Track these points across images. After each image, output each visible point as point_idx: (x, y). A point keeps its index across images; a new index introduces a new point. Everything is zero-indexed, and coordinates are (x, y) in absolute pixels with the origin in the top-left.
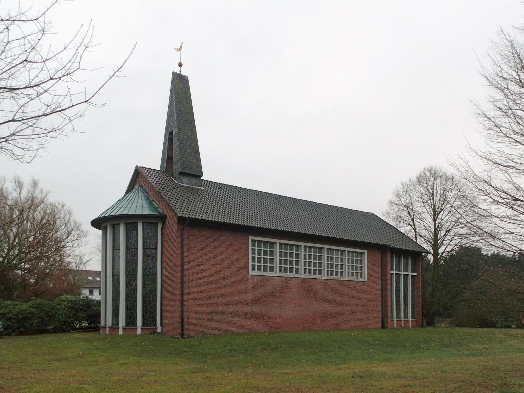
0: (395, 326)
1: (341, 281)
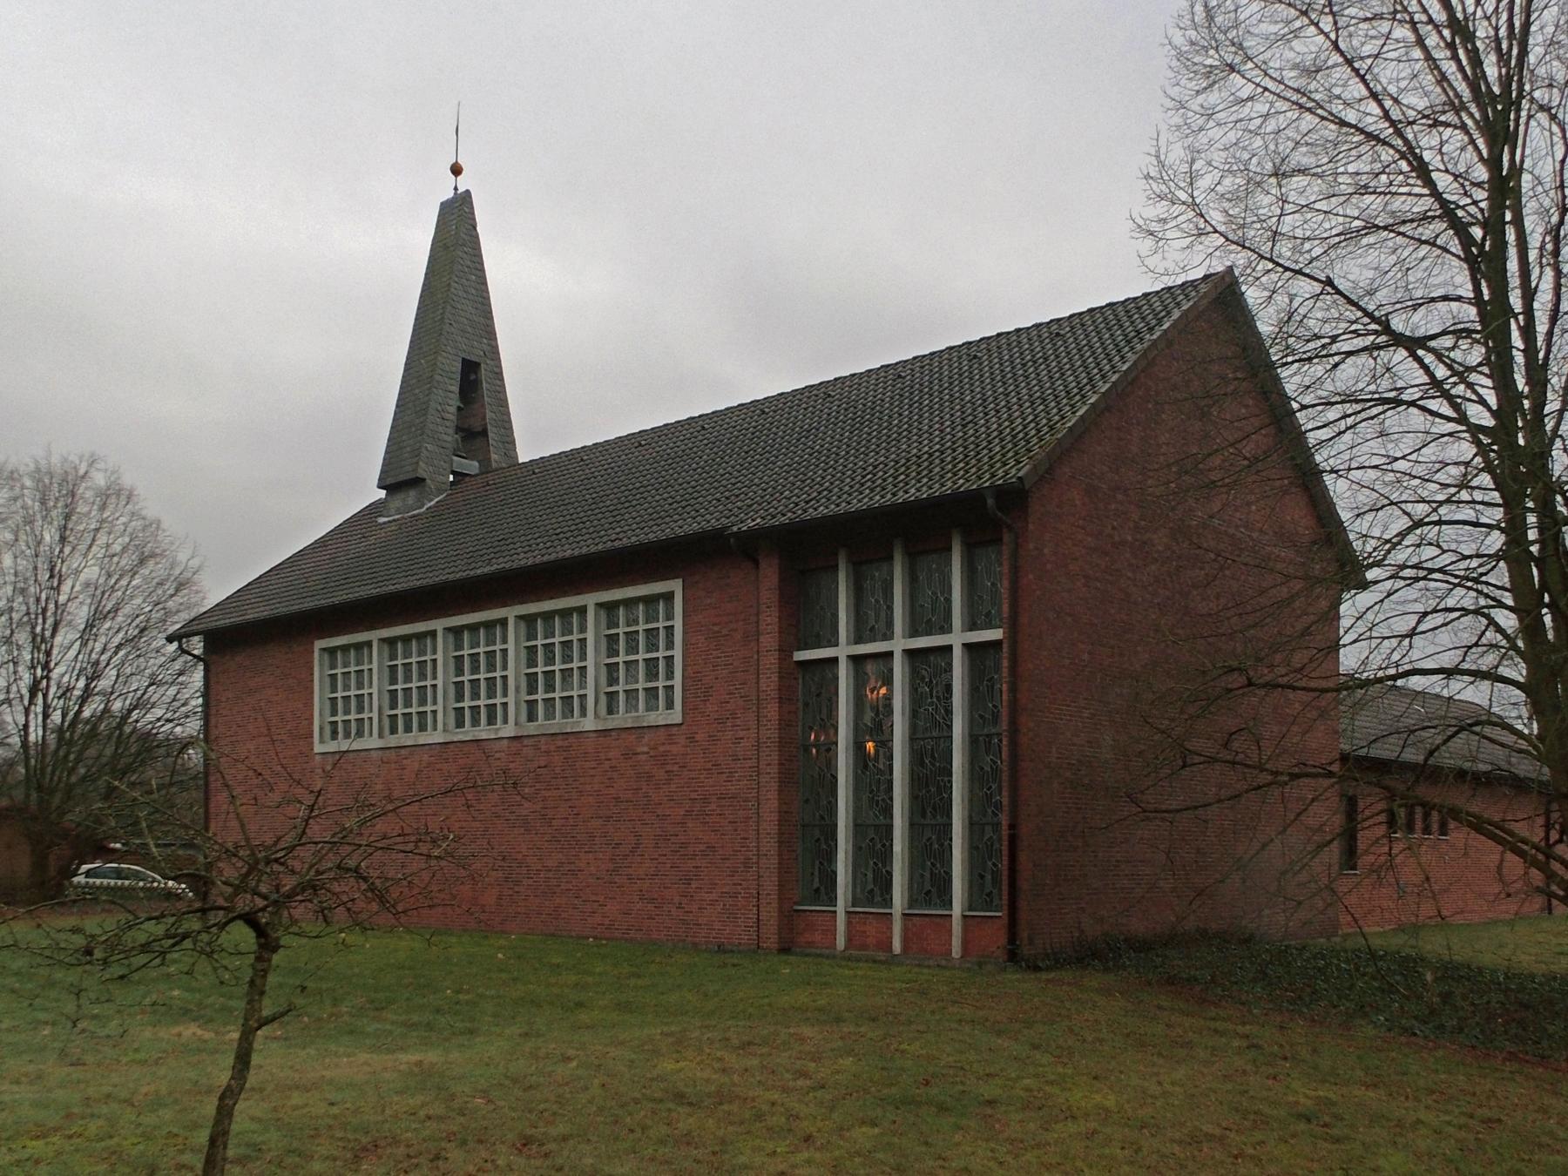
0: (841, 942)
1: (572, 739)
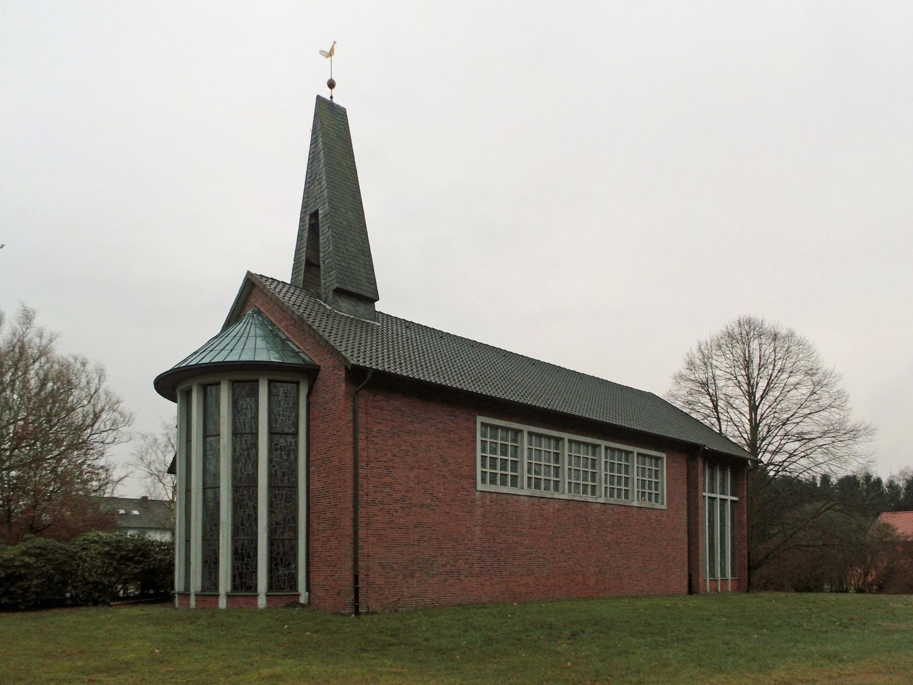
0: (708, 590)
1: (627, 508)
